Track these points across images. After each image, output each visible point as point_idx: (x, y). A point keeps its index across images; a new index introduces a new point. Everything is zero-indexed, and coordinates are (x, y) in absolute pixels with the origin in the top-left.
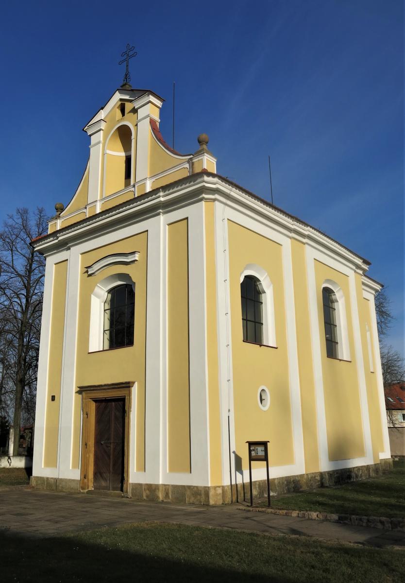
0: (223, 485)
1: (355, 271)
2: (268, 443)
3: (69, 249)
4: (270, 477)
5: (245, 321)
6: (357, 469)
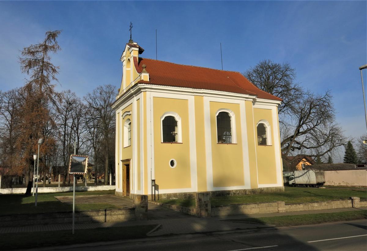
3: (119, 108)
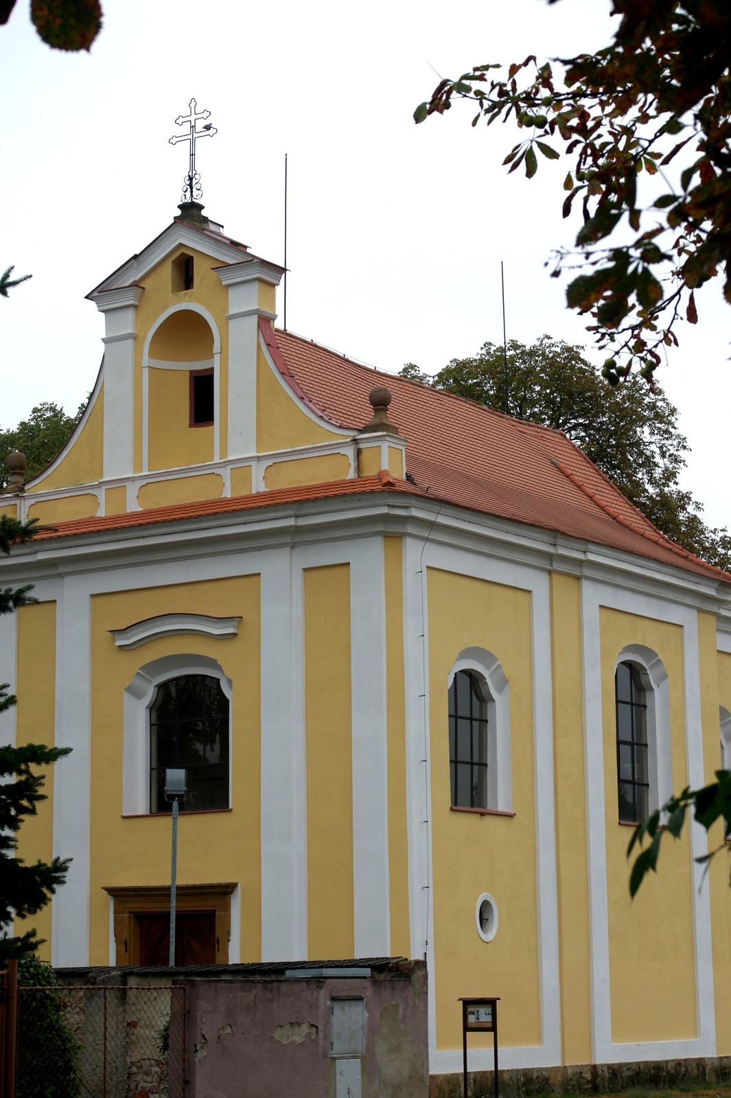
0: (593, 1063)
1: (700, 610)
2: (497, 1001)
4: (499, 1068)
5: (454, 764)
6: (674, 1064)
